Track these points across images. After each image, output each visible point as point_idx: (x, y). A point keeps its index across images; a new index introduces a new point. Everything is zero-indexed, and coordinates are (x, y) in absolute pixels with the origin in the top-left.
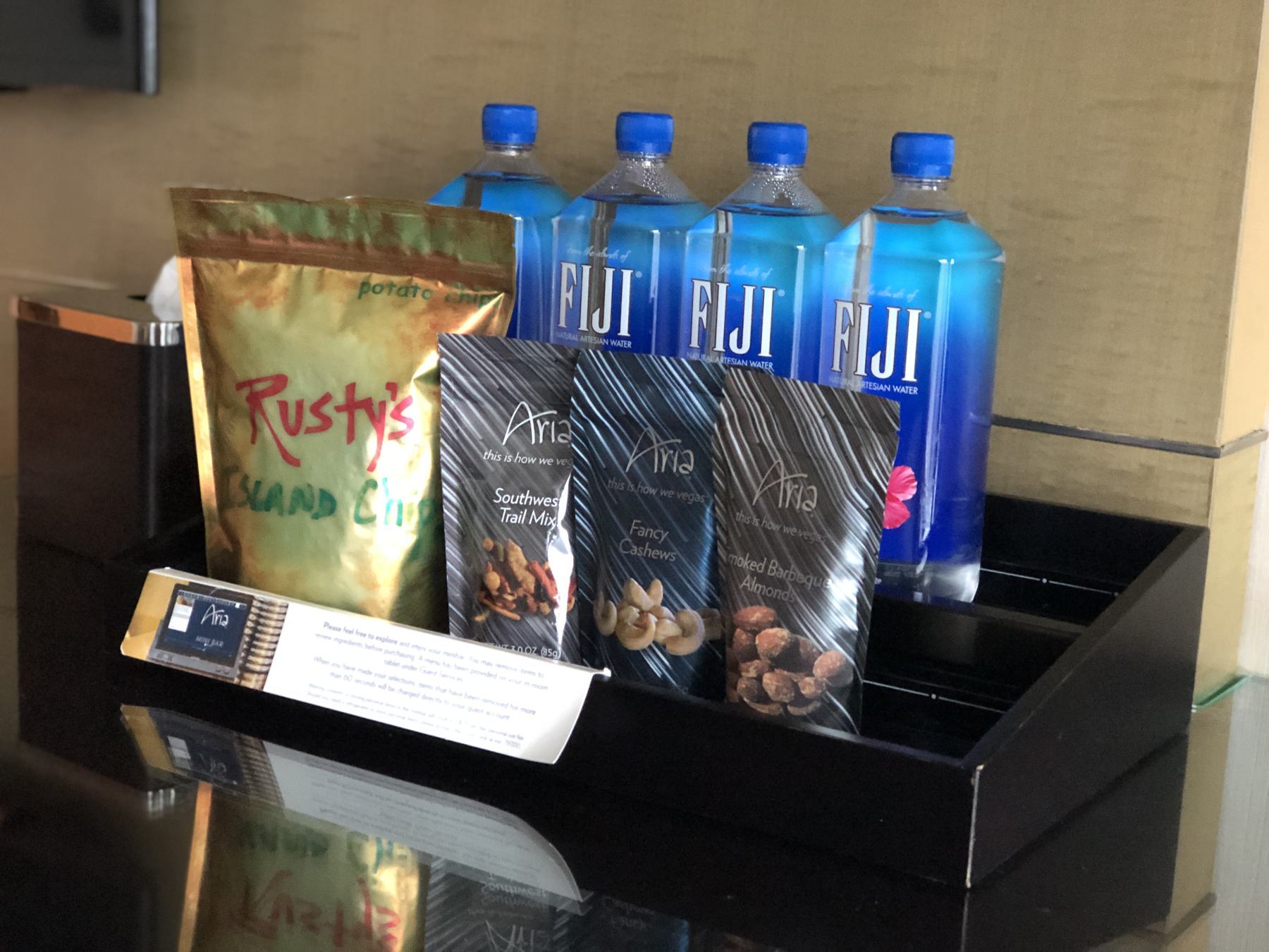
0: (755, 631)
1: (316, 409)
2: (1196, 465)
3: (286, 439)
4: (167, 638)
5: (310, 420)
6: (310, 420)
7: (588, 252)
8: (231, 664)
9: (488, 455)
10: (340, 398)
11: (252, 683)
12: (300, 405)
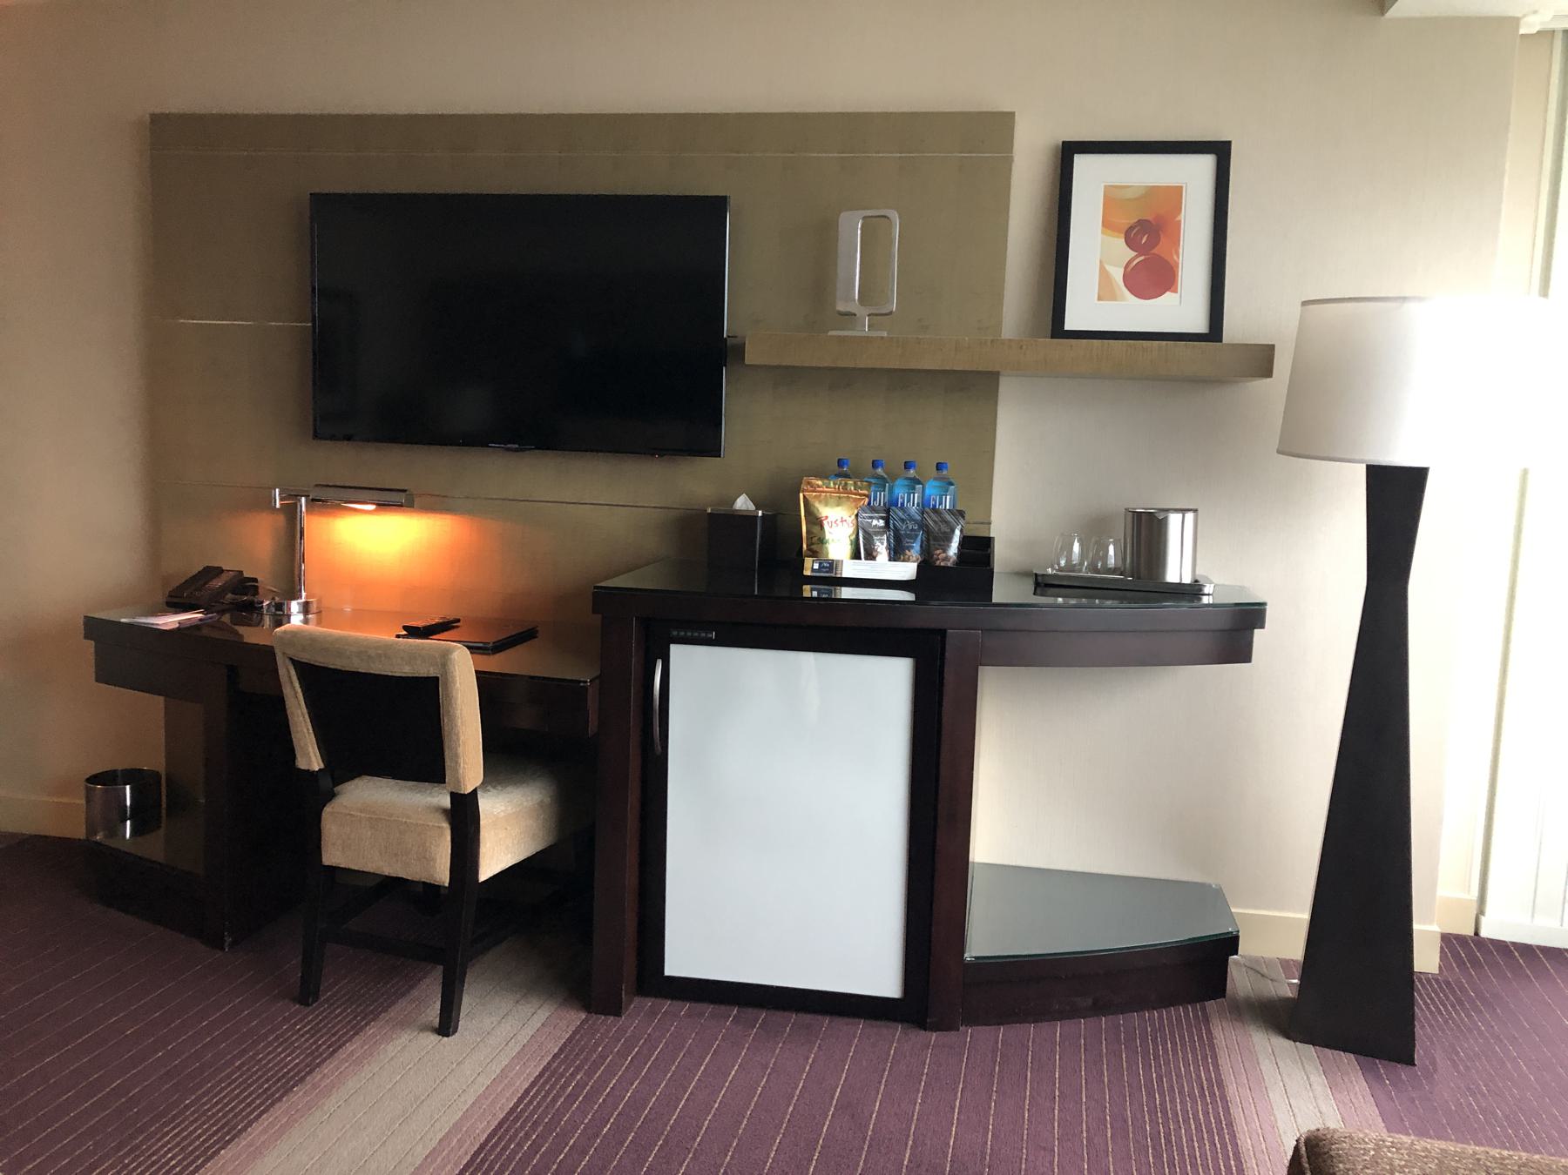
4: (813, 570)
10: (840, 520)
11: (839, 576)
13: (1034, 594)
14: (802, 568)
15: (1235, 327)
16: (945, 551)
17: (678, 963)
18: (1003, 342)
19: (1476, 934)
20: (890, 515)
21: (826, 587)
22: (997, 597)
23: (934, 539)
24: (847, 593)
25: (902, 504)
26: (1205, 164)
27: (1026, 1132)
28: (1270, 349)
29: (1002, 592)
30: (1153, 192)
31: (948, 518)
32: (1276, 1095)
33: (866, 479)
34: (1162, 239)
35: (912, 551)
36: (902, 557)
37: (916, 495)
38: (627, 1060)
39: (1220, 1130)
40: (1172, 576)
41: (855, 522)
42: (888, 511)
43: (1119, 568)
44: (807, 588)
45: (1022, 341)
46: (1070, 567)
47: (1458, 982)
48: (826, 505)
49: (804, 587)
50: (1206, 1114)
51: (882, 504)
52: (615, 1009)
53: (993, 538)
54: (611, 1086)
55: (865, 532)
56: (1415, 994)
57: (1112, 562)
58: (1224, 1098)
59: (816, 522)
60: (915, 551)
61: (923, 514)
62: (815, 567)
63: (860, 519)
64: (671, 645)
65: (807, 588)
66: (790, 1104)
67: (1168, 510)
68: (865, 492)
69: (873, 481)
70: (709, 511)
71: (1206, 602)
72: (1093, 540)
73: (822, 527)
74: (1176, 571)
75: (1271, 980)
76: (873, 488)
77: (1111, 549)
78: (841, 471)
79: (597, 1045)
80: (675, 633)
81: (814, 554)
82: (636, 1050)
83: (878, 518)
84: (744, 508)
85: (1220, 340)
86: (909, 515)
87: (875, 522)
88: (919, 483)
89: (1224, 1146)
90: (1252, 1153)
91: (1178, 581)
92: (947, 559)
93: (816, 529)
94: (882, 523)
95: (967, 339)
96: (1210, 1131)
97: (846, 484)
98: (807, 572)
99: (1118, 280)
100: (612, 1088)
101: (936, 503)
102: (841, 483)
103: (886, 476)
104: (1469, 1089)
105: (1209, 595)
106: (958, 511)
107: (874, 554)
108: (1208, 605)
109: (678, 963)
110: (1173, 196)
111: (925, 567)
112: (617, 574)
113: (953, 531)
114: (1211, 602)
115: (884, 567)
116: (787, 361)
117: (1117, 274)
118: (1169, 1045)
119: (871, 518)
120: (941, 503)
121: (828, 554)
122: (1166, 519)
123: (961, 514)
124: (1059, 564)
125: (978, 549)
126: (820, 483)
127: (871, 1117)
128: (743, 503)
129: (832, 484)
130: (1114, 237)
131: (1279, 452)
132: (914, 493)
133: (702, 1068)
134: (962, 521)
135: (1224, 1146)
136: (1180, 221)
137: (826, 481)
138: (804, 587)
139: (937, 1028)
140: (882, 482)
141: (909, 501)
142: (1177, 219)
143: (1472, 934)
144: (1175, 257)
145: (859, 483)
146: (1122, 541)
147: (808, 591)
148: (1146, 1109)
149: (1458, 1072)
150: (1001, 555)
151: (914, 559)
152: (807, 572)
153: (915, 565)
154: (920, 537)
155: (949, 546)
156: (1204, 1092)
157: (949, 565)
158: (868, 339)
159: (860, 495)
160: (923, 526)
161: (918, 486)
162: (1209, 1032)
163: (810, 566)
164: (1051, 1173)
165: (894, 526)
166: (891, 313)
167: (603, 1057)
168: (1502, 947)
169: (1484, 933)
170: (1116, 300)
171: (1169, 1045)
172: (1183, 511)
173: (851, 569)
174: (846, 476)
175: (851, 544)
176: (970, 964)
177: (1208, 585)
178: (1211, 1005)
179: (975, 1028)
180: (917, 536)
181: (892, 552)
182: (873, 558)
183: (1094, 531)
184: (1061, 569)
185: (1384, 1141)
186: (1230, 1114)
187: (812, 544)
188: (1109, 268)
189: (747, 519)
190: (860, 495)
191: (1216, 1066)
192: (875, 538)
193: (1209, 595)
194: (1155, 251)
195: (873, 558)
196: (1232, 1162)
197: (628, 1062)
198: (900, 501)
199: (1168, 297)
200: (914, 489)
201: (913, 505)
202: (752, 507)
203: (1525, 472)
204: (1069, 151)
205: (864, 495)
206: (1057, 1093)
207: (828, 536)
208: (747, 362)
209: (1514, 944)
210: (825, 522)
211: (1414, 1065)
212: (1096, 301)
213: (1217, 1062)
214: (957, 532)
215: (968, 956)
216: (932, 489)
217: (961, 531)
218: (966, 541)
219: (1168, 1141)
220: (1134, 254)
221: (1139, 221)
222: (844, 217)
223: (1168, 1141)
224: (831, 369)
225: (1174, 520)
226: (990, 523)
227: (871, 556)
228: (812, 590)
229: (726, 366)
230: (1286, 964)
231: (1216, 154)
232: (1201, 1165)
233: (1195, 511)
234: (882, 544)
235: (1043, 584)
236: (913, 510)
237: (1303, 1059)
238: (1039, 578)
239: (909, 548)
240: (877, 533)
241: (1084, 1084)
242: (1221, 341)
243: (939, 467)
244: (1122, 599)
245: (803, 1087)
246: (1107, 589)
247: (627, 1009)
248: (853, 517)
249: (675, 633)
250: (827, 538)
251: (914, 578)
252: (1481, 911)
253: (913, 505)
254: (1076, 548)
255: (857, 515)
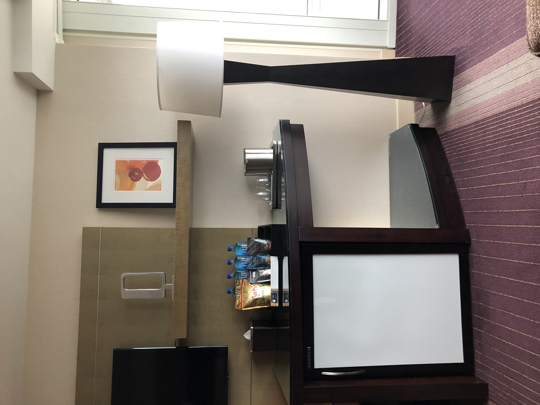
0: (266, 247)
1: (255, 293)
2: (254, 230)
3: (258, 295)
4: (276, 302)
5: (256, 294)
6: (256, 294)
7: (240, 263)
8: (277, 293)
9: (257, 278)
10: (253, 291)
11: (278, 290)
12: (255, 295)
13: (280, 209)
14: (275, 307)
15: (172, 138)
16: (265, 245)
17: (458, 357)
18: (177, 226)
19: (394, 49)
20: (250, 270)
21: (283, 296)
22: (285, 223)
23: (260, 250)
24: (286, 286)
25: (246, 264)
26: (107, 152)
27: (517, 195)
28: (180, 122)
29: (281, 220)
30: (118, 172)
31: (251, 245)
32: (479, 101)
33: (236, 281)
34: (136, 167)
35: (265, 259)
36: (268, 263)
37: (242, 259)
38: (512, 381)
39: (500, 118)
40: (271, 156)
41: (254, 284)
42: (249, 270)
43: (268, 177)
44: (284, 305)
45: (176, 219)
46: (268, 196)
47: (415, 50)
48: (247, 298)
49: (284, 306)
50: (494, 125)
51: (246, 273)
52: (484, 388)
53: (258, 226)
54: (528, 388)
55: (258, 280)
56: (427, 56)
57: (266, 180)
58: (483, 120)
59: (255, 302)
60: (265, 258)
61: (249, 255)
62: (275, 302)
63: (253, 282)
64: (315, 368)
65: (284, 305)
66: (523, 301)
67: (245, 160)
68: (241, 281)
69: (236, 278)
70: (252, 351)
71: (281, 143)
72: (257, 187)
73: (257, 299)
74: (268, 155)
75: (424, 113)
76: (240, 278)
77: (261, 180)
78: (232, 292)
79: (505, 395)
80: (309, 366)
81: (269, 302)
82: (505, 376)
83: (252, 275)
84: (250, 335)
85: (176, 143)
86: (250, 261)
87: (254, 276)
88: (236, 258)
89: (507, 116)
90: (509, 104)
91: (272, 154)
92: (268, 244)
93: (258, 302)
94: (254, 273)
95: (175, 241)
96: (501, 122)
97: (238, 289)
98: (277, 305)
99: (153, 184)
100: (530, 388)
101: (245, 250)
102: (237, 292)
103: (234, 272)
104: (463, 34)
105: (277, 142)
106: (248, 241)
107: (267, 275)
108: (282, 142)
109: (458, 357)
110: (119, 163)
111: (272, 253)
112: (282, 393)
113: (256, 242)
114: (281, 141)
115: (273, 271)
116: (185, 319)
117: (150, 184)
118: (461, 145)
119: (252, 277)
120: (245, 248)
121: (269, 296)
122: (249, 160)
123: (249, 239)
124: (268, 200)
125: (263, 232)
126: (238, 301)
127: (523, 263)
128: (248, 336)
129: (238, 296)
130: (135, 186)
131: (220, 117)
132: (241, 260)
133: (510, 344)
134: (252, 239)
135: (507, 116)
136: (130, 161)
137: (237, 298)
138: (284, 306)
139: (469, 239)
140: (237, 274)
141: (244, 262)
142: (129, 162)
143: (395, 50)
144: (144, 162)
145: (237, 284)
146: (257, 176)
147: (286, 304)
148: (495, 149)
149: (455, 40)
150: (265, 222)
151: (269, 258)
152: (277, 305)
153: (271, 257)
154: (259, 256)
155: (263, 244)
156: (482, 128)
157: (270, 243)
158: (175, 284)
159: (242, 283)
160: (254, 255)
161: (238, 259)
162: (453, 131)
163: (274, 304)
164: (538, 182)
165: (255, 267)
166: (165, 274)
167: (512, 393)
168: (398, 40)
169: (394, 46)
170: (161, 183)
171: (461, 145)
172: (245, 154)
173: (275, 285)
174: (234, 290)
175: (264, 286)
176: (440, 225)
177: (273, 142)
178: (439, 133)
179: (466, 223)
180: (259, 258)
181: (267, 268)
182: (269, 275)
183: (253, 188)
184: (270, 200)
185: (534, 17)
186: (491, 116)
187: (265, 303)
188: (147, 188)
189: (255, 334)
190: (242, 283)
191: (468, 126)
192: (261, 275)
193: (277, 142)
194: (141, 170)
195: (269, 275)
196: (516, 111)
197: (513, 380)
198: (244, 266)
199: (160, 164)
200: (239, 260)
201: (246, 260)
202: (249, 331)
203: (226, 40)
204: (100, 205)
205: (242, 281)
206: (494, 185)
207: (261, 296)
208: (185, 337)
209: (396, 36)
210: (255, 298)
211: (455, 56)
212: (161, 191)
213: (466, 125)
214: (257, 240)
215: (437, 227)
216: (239, 252)
217: (256, 239)
218: (260, 237)
219: (510, 137)
220: (142, 178)
221: (129, 176)
222: (124, 296)
223: (510, 137)
224: (189, 299)
225: (248, 157)
226: (252, 228)
227: (268, 277)
228: (285, 302)
229: (188, 347)
230: (417, 109)
231: (103, 148)
232: (520, 122)
233: (244, 149)
234: (263, 272)
235: (277, 206)
236: (248, 259)
237: (459, 94)
238: (274, 207)
239: (264, 260)
240: (259, 275)
241: (487, 175)
242: (177, 142)
243: (230, 250)
244: (281, 176)
245: (512, 296)
246: (277, 180)
247: (483, 381)
248: (252, 285)
249: (309, 366)
250: (261, 297)
251: (277, 257)
252: (386, 48)
253: (246, 260)
254: (260, 194)
255: (251, 284)
